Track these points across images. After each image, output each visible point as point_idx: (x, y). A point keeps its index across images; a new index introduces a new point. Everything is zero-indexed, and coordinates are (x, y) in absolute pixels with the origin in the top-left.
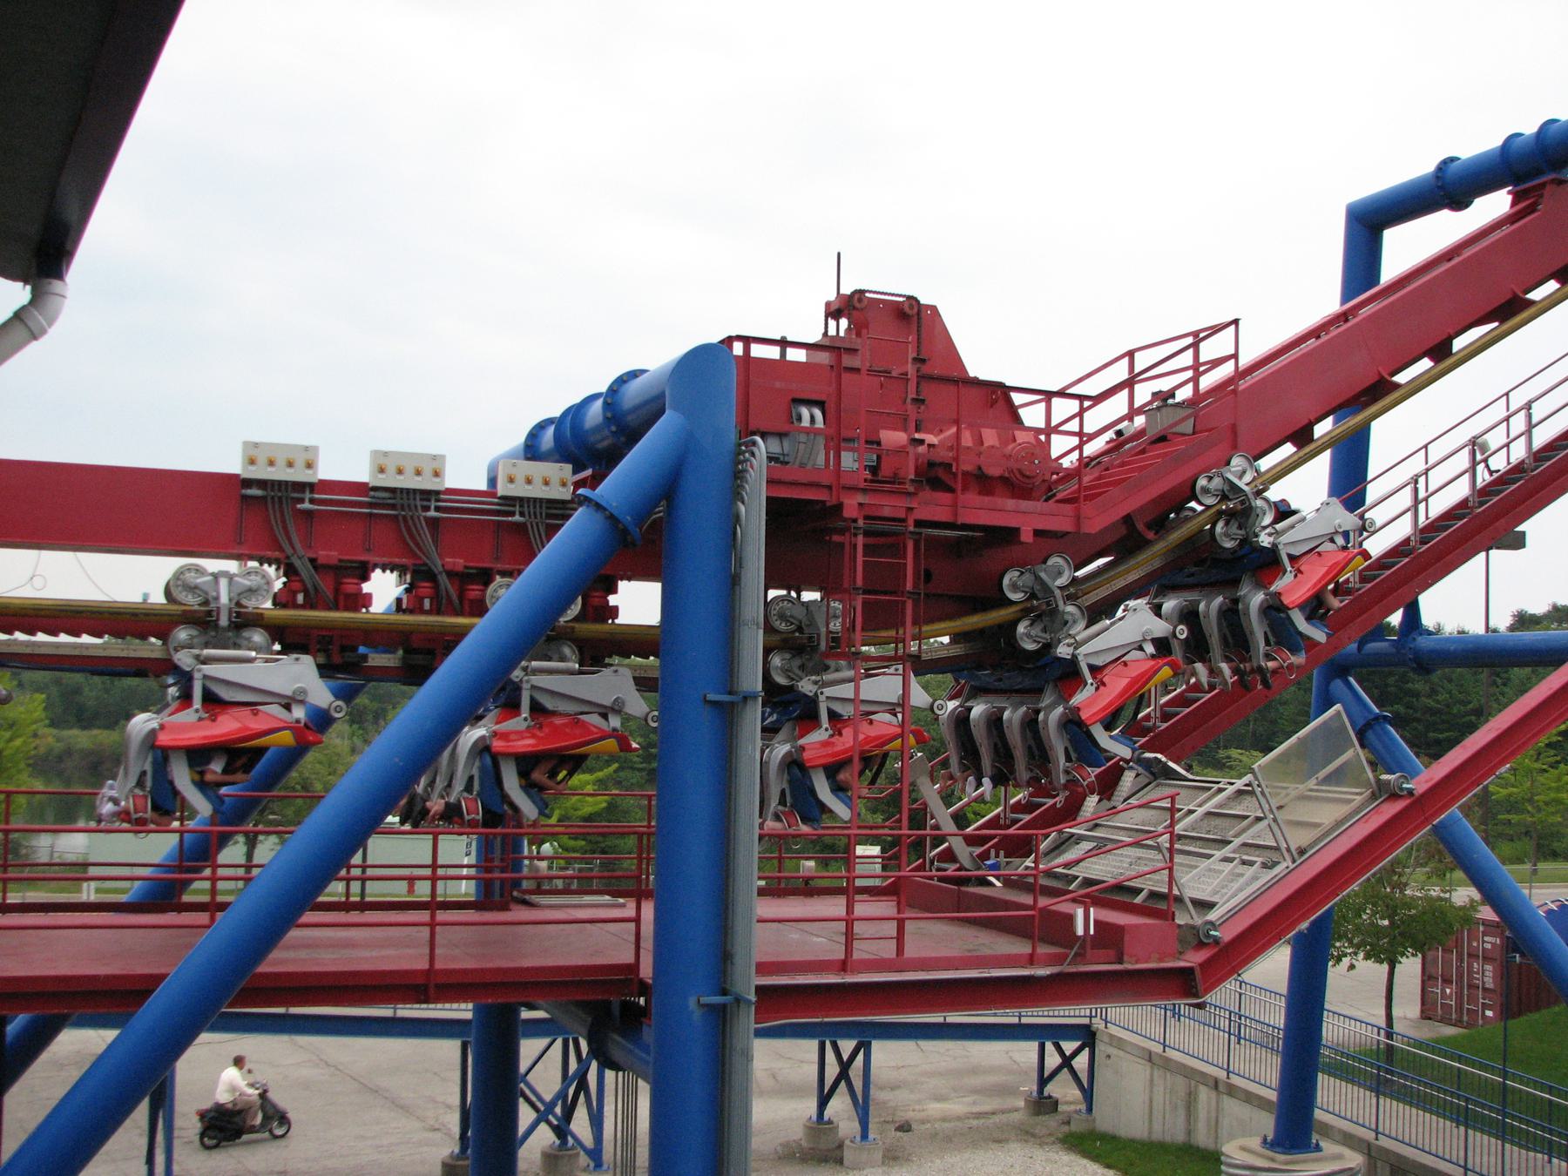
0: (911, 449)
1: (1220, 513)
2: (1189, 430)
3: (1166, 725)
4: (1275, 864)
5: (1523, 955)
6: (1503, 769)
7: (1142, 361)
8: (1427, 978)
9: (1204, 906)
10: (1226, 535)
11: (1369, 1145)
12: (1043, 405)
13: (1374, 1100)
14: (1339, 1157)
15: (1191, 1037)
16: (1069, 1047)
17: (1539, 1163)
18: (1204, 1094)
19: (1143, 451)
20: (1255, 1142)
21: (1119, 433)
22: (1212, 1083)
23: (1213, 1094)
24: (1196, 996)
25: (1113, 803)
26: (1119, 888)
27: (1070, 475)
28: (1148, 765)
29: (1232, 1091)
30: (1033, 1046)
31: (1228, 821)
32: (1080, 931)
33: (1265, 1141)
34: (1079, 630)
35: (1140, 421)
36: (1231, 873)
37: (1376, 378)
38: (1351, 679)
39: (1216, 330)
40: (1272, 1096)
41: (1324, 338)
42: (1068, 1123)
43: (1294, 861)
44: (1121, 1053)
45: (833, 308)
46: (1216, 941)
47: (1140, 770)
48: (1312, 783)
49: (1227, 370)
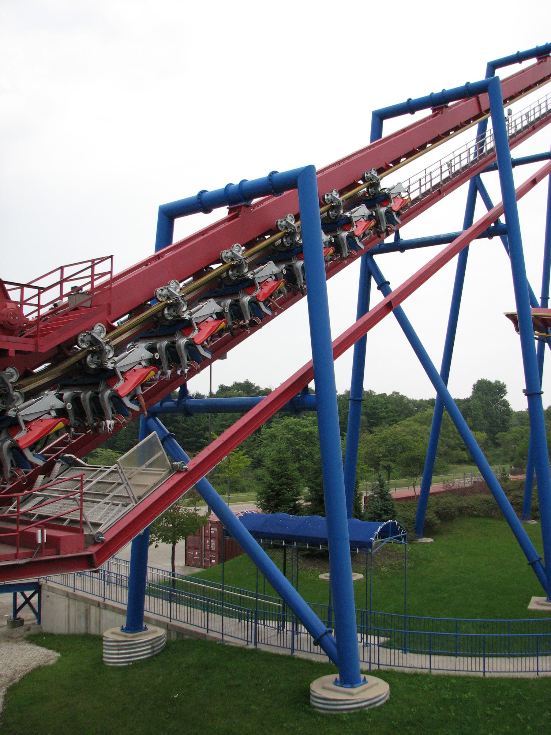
1: (89, 352)
2: (89, 305)
3: (75, 441)
4: (128, 504)
5: (230, 536)
6: (224, 458)
7: (67, 272)
8: (188, 548)
9: (96, 525)
10: (92, 362)
11: (167, 625)
12: (20, 290)
13: (169, 604)
14: (155, 632)
15: (86, 584)
16: (28, 593)
17: (237, 623)
18: (93, 609)
19: (66, 314)
20: (118, 629)
21: (56, 305)
22: (97, 605)
23: (98, 609)
24: (94, 567)
25: (51, 478)
26: (60, 519)
27: (31, 325)
28: (67, 460)
29: (106, 607)
30: (11, 594)
31: (105, 485)
32: (40, 541)
33: (122, 629)
34: (20, 404)
35: (65, 300)
36: (108, 509)
37: (412, 149)
38: (157, 418)
39: (103, 259)
40: (125, 608)
41: (150, 266)
42: (29, 630)
43: (136, 503)
44: (54, 594)
46: (103, 541)
47: (64, 463)
48: (144, 467)
49: (108, 277)
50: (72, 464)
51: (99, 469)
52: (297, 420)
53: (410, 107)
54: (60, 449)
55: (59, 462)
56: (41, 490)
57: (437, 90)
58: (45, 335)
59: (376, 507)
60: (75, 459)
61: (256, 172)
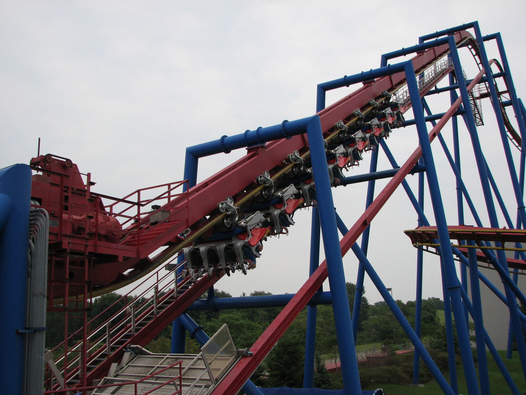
0: (87, 220)
28: (133, 349)
45: (35, 161)
47: (132, 352)
50: (138, 353)
51: (166, 357)
52: (230, 315)
53: (346, 82)
54: (126, 341)
55: (128, 351)
56: (117, 376)
57: (366, 70)
58: (144, 243)
59: (316, 379)
60: (141, 349)
61: (272, 120)
